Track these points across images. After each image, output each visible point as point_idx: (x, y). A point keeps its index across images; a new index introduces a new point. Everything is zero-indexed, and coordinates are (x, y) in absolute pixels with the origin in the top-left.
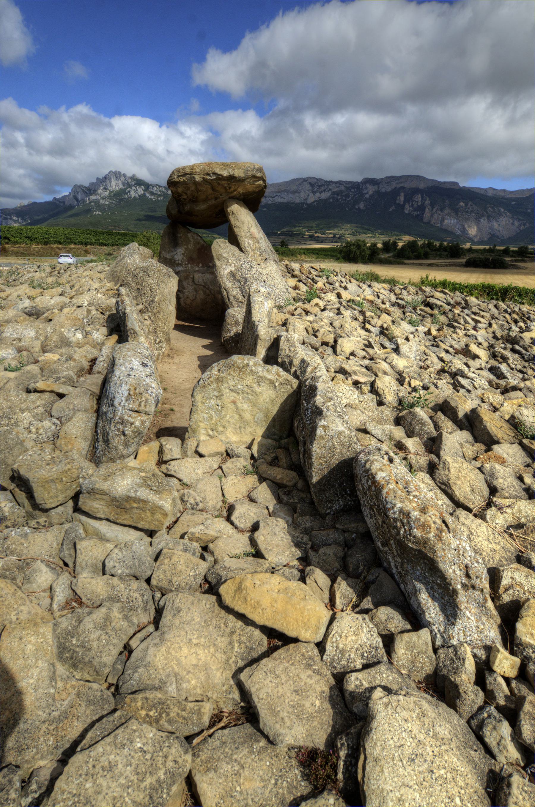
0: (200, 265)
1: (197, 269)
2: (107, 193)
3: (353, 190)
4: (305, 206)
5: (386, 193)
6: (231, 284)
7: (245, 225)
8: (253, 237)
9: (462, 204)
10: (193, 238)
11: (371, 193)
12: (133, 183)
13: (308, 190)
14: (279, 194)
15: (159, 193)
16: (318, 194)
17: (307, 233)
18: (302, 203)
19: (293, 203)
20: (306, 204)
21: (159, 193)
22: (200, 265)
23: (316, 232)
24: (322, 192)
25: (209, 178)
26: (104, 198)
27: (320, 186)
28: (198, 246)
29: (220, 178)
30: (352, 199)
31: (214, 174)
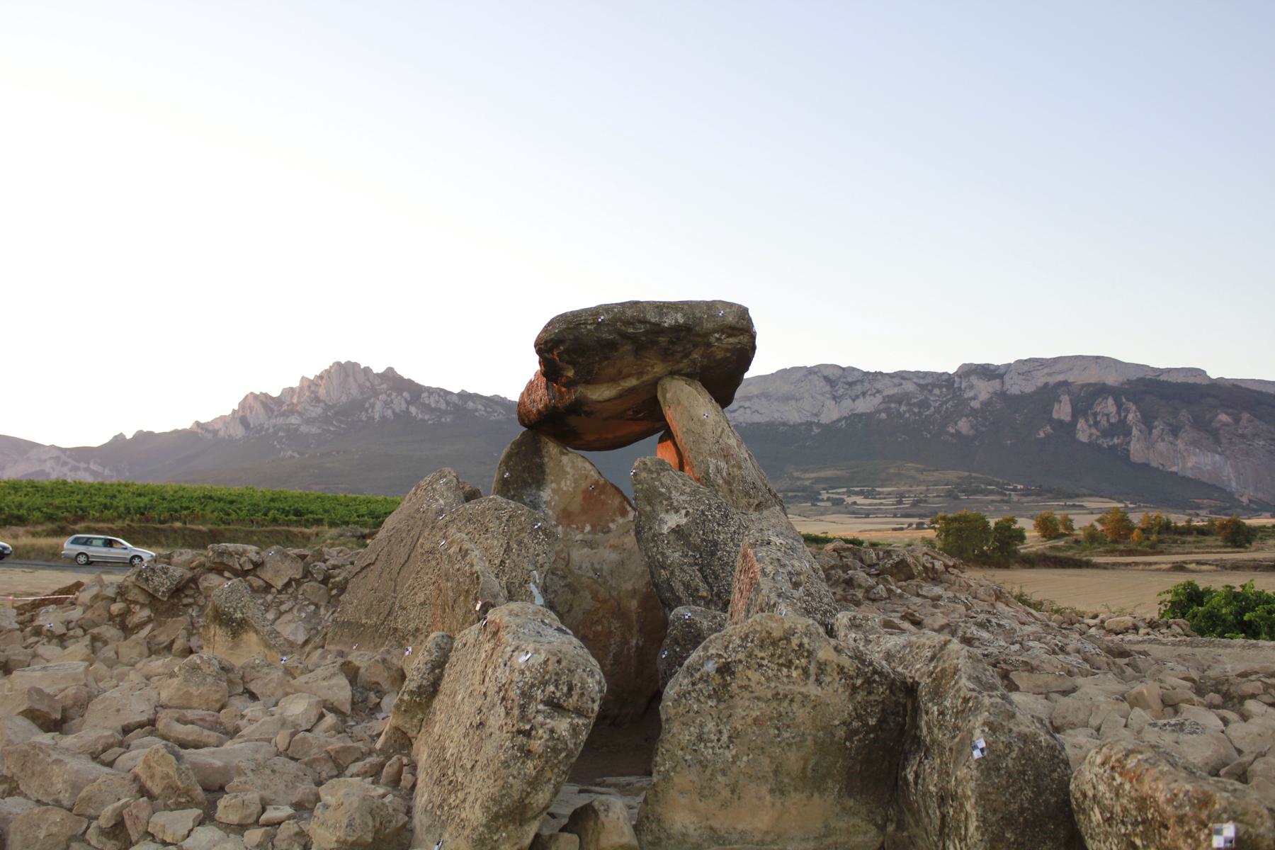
0: (588, 528)
1: (579, 537)
2: (319, 410)
3: (937, 391)
4: (816, 430)
5: (1022, 397)
6: (677, 555)
7: (709, 428)
8: (726, 455)
9: (1223, 417)
10: (573, 467)
11: (984, 396)
12: (384, 386)
13: (822, 394)
14: (747, 404)
15: (443, 406)
16: (847, 403)
17: (824, 495)
18: (810, 424)
19: (784, 424)
20: (819, 425)
21: (443, 406)
22: (588, 528)
23: (850, 493)
24: (857, 397)
25: (630, 330)
26: (309, 421)
27: (850, 384)
28: (584, 485)
29: (657, 330)
30: (938, 410)
31: (644, 322)
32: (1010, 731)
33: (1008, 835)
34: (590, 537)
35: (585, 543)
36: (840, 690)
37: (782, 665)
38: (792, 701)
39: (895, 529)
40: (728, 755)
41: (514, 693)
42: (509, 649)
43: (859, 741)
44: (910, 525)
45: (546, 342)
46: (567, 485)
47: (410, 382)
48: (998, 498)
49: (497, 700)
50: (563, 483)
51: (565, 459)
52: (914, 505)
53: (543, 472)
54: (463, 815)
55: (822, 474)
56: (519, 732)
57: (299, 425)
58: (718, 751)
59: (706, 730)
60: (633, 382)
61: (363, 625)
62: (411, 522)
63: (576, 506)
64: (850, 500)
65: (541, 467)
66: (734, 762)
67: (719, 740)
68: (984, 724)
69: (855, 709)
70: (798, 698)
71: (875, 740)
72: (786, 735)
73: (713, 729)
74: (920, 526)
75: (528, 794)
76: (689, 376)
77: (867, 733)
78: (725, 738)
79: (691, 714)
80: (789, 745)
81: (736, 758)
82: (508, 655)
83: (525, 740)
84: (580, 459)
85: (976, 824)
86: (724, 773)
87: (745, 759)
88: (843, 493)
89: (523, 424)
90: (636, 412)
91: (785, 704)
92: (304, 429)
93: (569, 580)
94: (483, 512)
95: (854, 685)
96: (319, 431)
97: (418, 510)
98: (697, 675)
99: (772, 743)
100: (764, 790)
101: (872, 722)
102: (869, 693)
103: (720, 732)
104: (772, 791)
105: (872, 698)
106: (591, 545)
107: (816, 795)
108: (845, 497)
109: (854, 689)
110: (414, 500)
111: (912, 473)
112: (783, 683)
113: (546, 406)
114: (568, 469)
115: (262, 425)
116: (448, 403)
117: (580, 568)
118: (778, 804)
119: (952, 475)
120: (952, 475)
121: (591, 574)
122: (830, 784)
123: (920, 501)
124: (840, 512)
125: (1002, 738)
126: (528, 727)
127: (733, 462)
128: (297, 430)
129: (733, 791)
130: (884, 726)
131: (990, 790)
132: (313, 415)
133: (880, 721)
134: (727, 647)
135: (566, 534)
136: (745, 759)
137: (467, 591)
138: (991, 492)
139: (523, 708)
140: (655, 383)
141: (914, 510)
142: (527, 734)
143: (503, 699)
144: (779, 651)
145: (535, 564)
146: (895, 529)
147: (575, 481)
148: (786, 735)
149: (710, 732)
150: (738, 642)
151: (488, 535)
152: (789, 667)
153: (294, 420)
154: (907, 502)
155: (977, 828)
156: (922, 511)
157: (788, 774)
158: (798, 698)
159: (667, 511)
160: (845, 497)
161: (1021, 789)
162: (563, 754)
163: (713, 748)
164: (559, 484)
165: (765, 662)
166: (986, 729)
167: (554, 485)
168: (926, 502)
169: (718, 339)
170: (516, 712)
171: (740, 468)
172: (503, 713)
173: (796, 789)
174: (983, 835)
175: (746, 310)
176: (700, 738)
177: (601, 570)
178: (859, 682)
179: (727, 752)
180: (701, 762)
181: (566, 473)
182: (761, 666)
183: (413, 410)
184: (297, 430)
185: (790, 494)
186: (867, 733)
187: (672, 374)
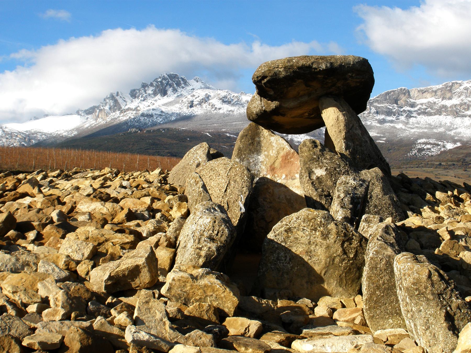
0: (284, 176)
28: (282, 153)
33: (377, 293)
37: (313, 230)
38: (316, 245)
40: (289, 266)
41: (197, 234)
42: (198, 217)
43: (346, 263)
46: (273, 153)
49: (191, 236)
50: (271, 151)
53: (261, 146)
56: (197, 248)
58: (285, 264)
59: (280, 255)
62: (184, 170)
66: (291, 270)
67: (285, 260)
68: (375, 251)
71: (352, 264)
73: (283, 255)
77: (349, 261)
78: (288, 259)
79: (274, 249)
81: (292, 267)
82: (197, 220)
83: (199, 251)
84: (281, 139)
85: (365, 287)
89: (250, 120)
90: (310, 114)
97: (188, 164)
98: (277, 232)
103: (286, 257)
104: (307, 282)
110: (187, 159)
117: (279, 198)
122: (332, 281)
125: (380, 256)
126: (201, 246)
129: (291, 282)
131: (372, 275)
134: (290, 221)
136: (296, 268)
137: (197, 200)
139: (199, 240)
142: (200, 249)
143: (193, 236)
144: (311, 224)
145: (242, 192)
149: (282, 256)
150: (295, 219)
151: (220, 177)
152: (315, 231)
155: (366, 289)
159: (316, 168)
161: (385, 276)
163: (283, 263)
164: (268, 152)
165: (305, 228)
166: (375, 253)
167: (266, 153)
169: (351, 77)
170: (197, 241)
172: (192, 242)
174: (367, 292)
176: (278, 259)
179: (288, 265)
180: (277, 269)
181: (273, 146)
182: (304, 230)
185: (449, 163)
186: (349, 261)
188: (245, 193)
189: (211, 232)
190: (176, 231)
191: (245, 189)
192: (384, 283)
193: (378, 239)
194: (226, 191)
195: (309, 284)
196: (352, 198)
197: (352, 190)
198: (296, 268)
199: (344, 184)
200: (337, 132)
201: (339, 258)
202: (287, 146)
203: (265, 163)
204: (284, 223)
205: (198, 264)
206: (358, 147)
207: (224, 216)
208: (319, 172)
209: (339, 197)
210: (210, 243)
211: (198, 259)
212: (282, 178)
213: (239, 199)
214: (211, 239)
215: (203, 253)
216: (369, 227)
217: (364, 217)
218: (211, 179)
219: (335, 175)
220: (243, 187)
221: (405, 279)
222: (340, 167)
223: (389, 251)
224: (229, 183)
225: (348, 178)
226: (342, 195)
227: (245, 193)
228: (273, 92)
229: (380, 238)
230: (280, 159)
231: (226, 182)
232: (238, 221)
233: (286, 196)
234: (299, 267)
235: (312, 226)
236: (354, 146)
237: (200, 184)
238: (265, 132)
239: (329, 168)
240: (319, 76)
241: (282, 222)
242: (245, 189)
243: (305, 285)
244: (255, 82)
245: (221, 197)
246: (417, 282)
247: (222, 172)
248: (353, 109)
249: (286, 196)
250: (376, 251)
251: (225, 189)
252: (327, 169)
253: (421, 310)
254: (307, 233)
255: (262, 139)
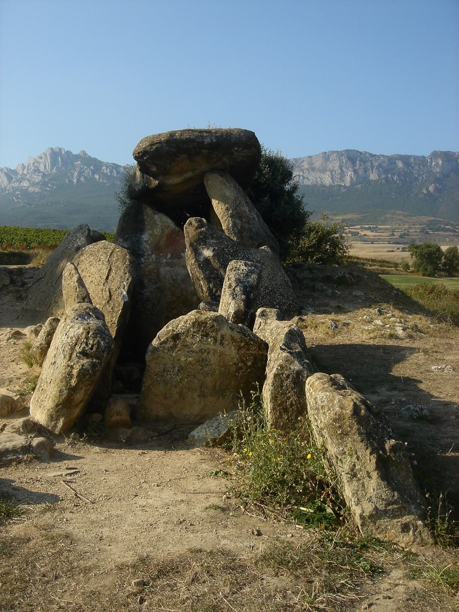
0: (169, 256)
1: (164, 261)
22: (169, 256)
23: (363, 229)
26: (34, 184)
28: (167, 231)
32: (290, 369)
34: (170, 261)
35: (168, 264)
36: (233, 348)
38: (208, 353)
39: (389, 251)
42: (68, 327)
44: (398, 249)
45: (139, 153)
46: (157, 232)
47: (95, 160)
48: (452, 234)
50: (155, 230)
51: (156, 217)
52: (401, 236)
54: (45, 404)
55: (346, 217)
57: (28, 187)
59: (167, 366)
60: (190, 174)
61: (37, 311)
63: (162, 243)
64: (362, 233)
65: (142, 222)
66: (181, 382)
69: (240, 357)
70: (212, 352)
72: (206, 369)
74: (404, 250)
75: (72, 394)
76: (222, 171)
80: (207, 374)
86: (176, 387)
87: (186, 380)
88: (359, 229)
91: (205, 355)
92: (31, 189)
93: (158, 285)
94: (98, 251)
95: (240, 346)
96: (40, 190)
99: (199, 373)
100: (196, 395)
101: (249, 364)
102: (248, 350)
104: (199, 396)
105: (248, 352)
106: (171, 265)
107: (221, 398)
108: (359, 231)
109: (240, 348)
111: (401, 217)
112: (204, 344)
113: (142, 187)
114: (158, 223)
115: (5, 188)
116: (118, 173)
117: (165, 278)
118: (202, 402)
119: (425, 219)
120: (425, 219)
121: (171, 281)
123: (404, 234)
124: (356, 240)
127: (244, 220)
128: (27, 190)
129: (180, 396)
130: (255, 366)
132: (37, 181)
133: (253, 364)
134: (178, 326)
135: (157, 259)
138: (448, 230)
140: (202, 175)
141: (401, 240)
142: (72, 367)
143: (64, 351)
146: (389, 251)
147: (162, 230)
148: (206, 369)
153: (25, 184)
154: (397, 235)
156: (405, 241)
157: (207, 388)
158: (212, 352)
160: (359, 231)
162: (88, 376)
163: (170, 375)
164: (153, 231)
167: (150, 232)
168: (408, 235)
170: (68, 357)
171: (249, 223)
172: (63, 358)
173: (211, 395)
175: (254, 133)
177: (177, 279)
178: (242, 344)
183: (97, 177)
184: (27, 190)
186: (246, 369)
187: (213, 170)
188: (128, 279)
189: (84, 345)
190: (47, 336)
191: (127, 275)
192: (291, 405)
193: (281, 349)
194: (107, 278)
195: (202, 397)
196: (245, 287)
197: (244, 277)
198: (186, 380)
199: (235, 271)
200: (224, 209)
201: (235, 366)
202: (171, 224)
203: (149, 242)
204: (170, 328)
205: (71, 385)
206: (246, 224)
207: (99, 323)
208: (208, 253)
209: (230, 286)
210: (83, 360)
211: (70, 380)
212: (168, 257)
213: (122, 286)
214: (84, 354)
215: (75, 372)
216: (266, 323)
217: (259, 310)
218: (91, 265)
219: (223, 255)
220: (126, 273)
221: (324, 413)
222: (228, 247)
223: (296, 366)
224: (111, 269)
225: (239, 264)
226: (234, 285)
227: (128, 279)
228: (155, 169)
229: (284, 347)
230: (164, 239)
231: (107, 268)
232: (121, 311)
233: (172, 276)
234: (189, 379)
235: (203, 331)
236: (241, 224)
237: (75, 278)
238: (149, 211)
239: (216, 248)
240: (203, 151)
241: (167, 327)
242: (127, 275)
243: (197, 399)
244: (136, 158)
245: (102, 284)
246: (339, 419)
247: (102, 257)
248: (239, 185)
249: (172, 276)
250: (281, 366)
251: (106, 276)
252: (214, 249)
253: (345, 452)
254: (198, 339)
255: (145, 217)
